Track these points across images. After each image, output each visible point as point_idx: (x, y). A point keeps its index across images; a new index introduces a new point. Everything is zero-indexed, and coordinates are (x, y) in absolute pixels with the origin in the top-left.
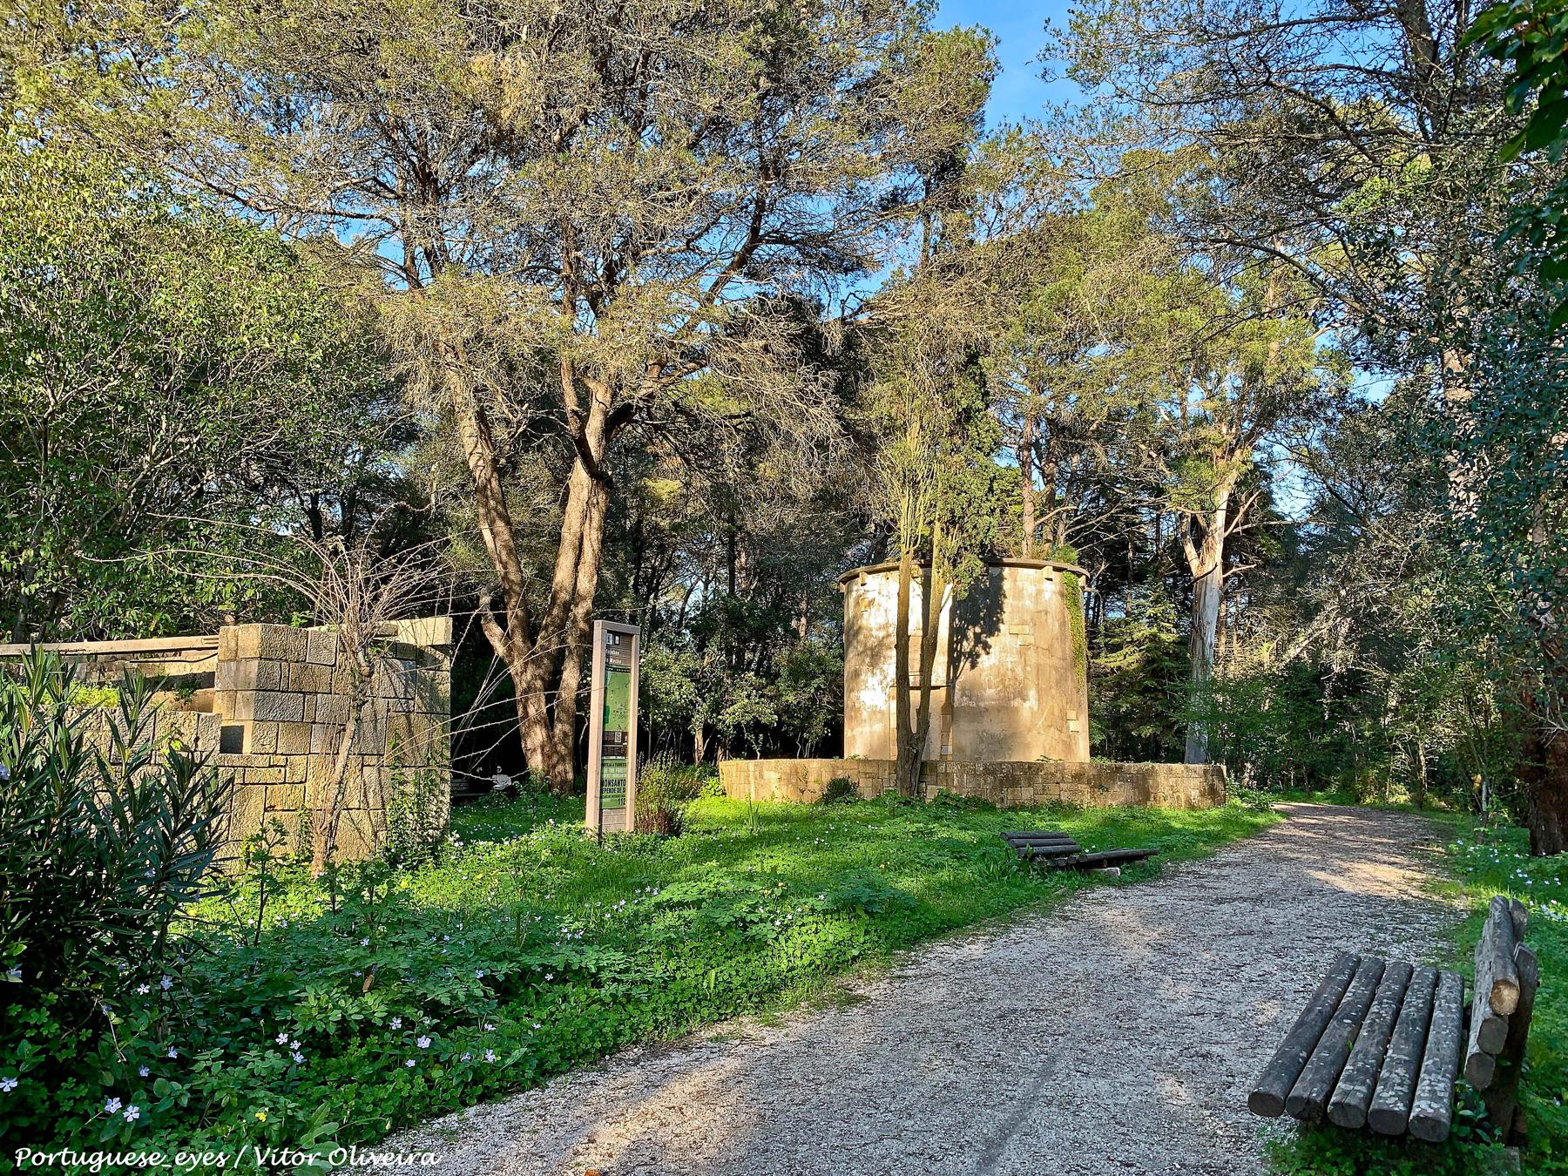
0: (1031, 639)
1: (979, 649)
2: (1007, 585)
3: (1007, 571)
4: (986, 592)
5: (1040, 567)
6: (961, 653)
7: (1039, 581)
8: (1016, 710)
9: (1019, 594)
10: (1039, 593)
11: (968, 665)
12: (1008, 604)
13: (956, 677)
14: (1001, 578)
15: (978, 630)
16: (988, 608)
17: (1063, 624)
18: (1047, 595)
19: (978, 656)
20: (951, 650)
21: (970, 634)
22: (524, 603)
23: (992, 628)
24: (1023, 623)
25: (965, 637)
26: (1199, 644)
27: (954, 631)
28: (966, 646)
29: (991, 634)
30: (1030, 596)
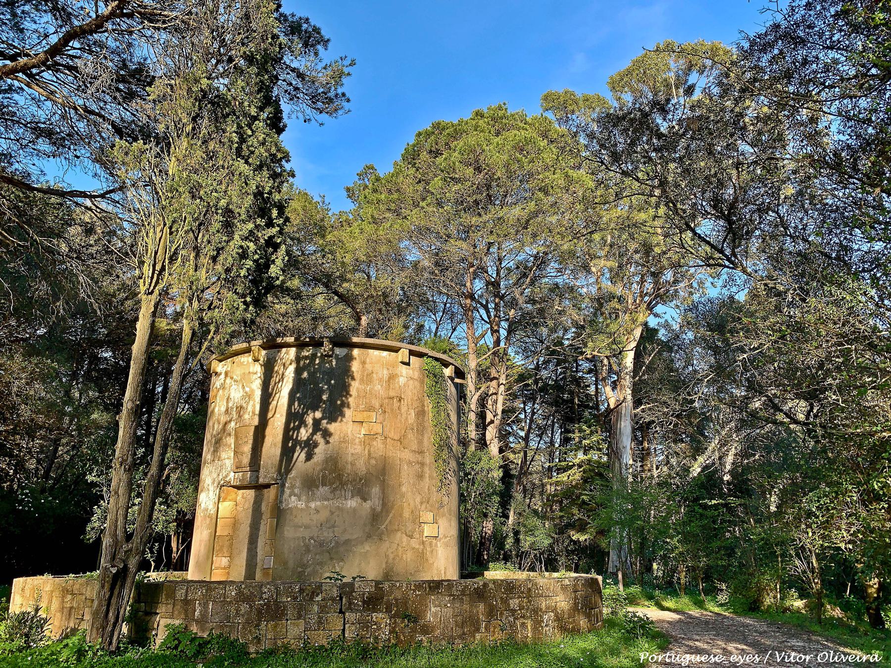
0: (378, 428)
1: (318, 437)
2: (355, 366)
3: (356, 352)
4: (330, 373)
5: (396, 350)
6: (297, 442)
7: (391, 365)
8: (350, 385)
9: (368, 378)
10: (392, 377)
11: (303, 456)
12: (355, 387)
13: (288, 471)
14: (349, 358)
15: (318, 415)
16: (331, 389)
17: (421, 413)
18: (402, 380)
19: (316, 445)
20: (287, 437)
21: (309, 420)
22: (288, 253)
23: (335, 412)
24: (370, 409)
25: (303, 423)
26: (617, 465)
27: (292, 416)
28: (304, 434)
29: (332, 419)
30: (380, 380)
